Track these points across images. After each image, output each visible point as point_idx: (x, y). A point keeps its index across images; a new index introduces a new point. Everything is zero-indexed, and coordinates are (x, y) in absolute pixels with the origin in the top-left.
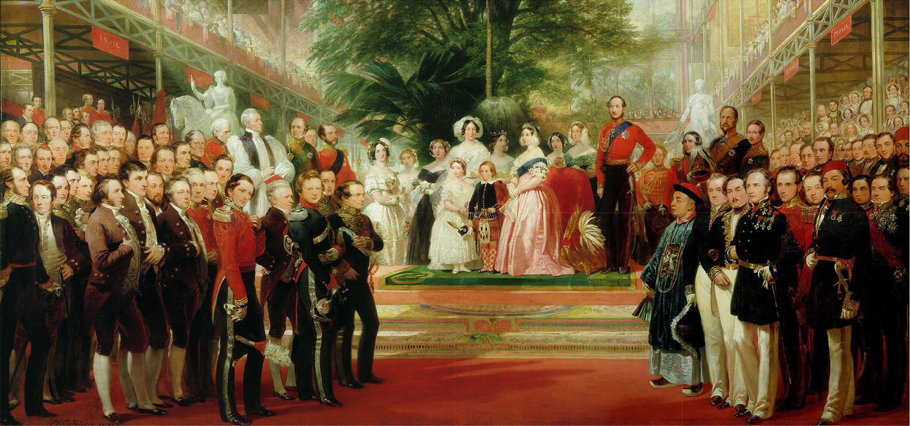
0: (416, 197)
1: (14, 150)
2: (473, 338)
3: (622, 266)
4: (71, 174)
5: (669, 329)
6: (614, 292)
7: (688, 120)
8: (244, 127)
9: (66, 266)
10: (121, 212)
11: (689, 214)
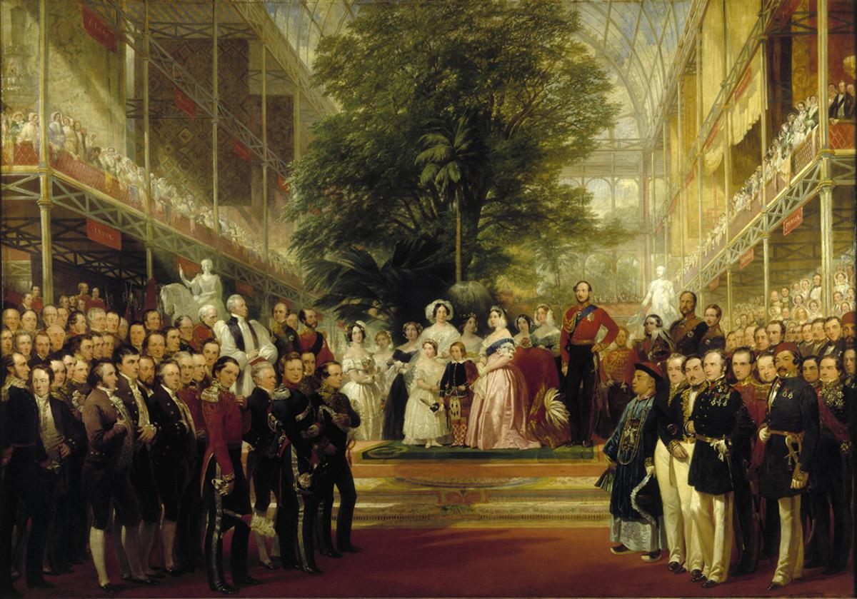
0: (390, 376)
1: (15, 337)
2: (445, 509)
3: (585, 439)
4: (68, 359)
5: (629, 499)
6: (578, 464)
7: (650, 304)
8: (230, 312)
9: (64, 445)
10: (115, 393)
11: (650, 391)
